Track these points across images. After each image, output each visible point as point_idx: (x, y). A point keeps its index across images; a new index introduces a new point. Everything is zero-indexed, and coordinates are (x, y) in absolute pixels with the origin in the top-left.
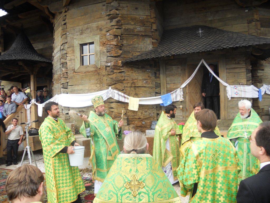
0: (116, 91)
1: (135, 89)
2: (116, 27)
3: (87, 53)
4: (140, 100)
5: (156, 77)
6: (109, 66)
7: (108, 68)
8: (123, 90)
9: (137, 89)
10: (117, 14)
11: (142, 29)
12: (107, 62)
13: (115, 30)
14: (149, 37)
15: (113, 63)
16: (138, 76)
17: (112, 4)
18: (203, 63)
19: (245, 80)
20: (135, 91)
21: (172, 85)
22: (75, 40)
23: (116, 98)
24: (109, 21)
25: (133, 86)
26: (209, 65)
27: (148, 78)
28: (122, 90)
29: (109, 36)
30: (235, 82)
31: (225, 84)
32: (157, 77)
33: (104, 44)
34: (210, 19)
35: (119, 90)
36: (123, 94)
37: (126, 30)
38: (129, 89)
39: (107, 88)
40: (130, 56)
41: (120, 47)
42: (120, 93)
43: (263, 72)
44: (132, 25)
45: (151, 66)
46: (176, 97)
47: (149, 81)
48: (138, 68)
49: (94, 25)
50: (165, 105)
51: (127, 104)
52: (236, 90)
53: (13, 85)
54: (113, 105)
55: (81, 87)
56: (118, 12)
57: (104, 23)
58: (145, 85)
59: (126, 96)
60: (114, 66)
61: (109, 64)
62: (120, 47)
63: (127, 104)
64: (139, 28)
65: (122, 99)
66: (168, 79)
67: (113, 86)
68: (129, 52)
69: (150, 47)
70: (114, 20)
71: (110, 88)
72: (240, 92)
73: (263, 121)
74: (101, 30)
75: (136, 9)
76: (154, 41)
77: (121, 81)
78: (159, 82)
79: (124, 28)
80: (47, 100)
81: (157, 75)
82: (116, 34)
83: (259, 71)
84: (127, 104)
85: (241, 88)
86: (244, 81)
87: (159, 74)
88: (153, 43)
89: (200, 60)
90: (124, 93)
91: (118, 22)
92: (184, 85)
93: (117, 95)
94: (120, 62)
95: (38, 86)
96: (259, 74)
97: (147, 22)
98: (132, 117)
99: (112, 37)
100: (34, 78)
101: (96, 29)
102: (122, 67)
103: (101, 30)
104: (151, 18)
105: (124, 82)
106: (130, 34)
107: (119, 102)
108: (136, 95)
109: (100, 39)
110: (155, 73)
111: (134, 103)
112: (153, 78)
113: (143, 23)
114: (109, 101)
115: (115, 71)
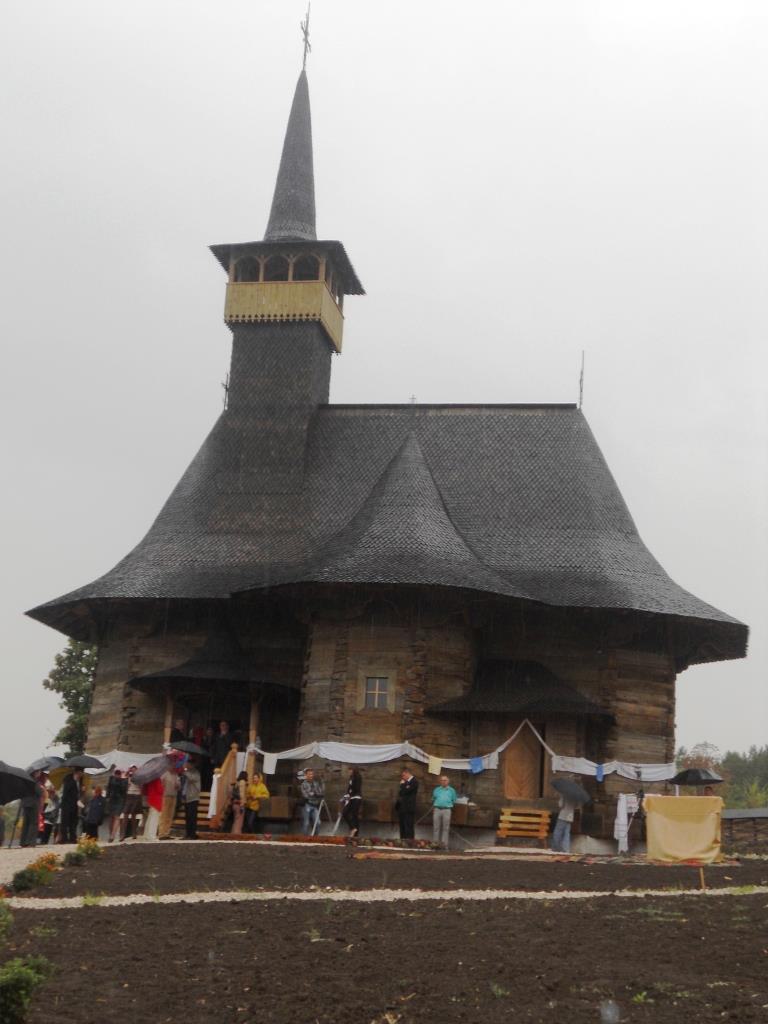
0: (414, 747)
2: (421, 663)
3: (374, 690)
5: (465, 734)
6: (407, 714)
7: (405, 716)
12: (405, 708)
15: (413, 711)
16: (442, 732)
18: (526, 724)
22: (360, 671)
23: (414, 755)
26: (533, 724)
30: (563, 753)
31: (551, 752)
33: (402, 683)
35: (417, 746)
36: (422, 752)
39: (403, 742)
41: (422, 690)
42: (419, 750)
46: (489, 764)
50: (475, 772)
52: (563, 763)
53: (727, 807)
54: (408, 765)
55: (362, 737)
59: (426, 754)
60: (414, 714)
61: (407, 711)
62: (422, 690)
66: (481, 739)
69: (460, 693)
70: (419, 653)
71: (407, 742)
72: (566, 766)
74: (399, 664)
76: (465, 684)
77: (421, 735)
80: (614, 814)
85: (569, 760)
86: (573, 751)
88: (465, 688)
90: (424, 751)
92: (500, 749)
93: (414, 752)
95: (733, 814)
96: (608, 746)
99: (415, 676)
103: (399, 664)
107: (416, 761)
108: (438, 755)
114: (405, 758)
115: (415, 721)
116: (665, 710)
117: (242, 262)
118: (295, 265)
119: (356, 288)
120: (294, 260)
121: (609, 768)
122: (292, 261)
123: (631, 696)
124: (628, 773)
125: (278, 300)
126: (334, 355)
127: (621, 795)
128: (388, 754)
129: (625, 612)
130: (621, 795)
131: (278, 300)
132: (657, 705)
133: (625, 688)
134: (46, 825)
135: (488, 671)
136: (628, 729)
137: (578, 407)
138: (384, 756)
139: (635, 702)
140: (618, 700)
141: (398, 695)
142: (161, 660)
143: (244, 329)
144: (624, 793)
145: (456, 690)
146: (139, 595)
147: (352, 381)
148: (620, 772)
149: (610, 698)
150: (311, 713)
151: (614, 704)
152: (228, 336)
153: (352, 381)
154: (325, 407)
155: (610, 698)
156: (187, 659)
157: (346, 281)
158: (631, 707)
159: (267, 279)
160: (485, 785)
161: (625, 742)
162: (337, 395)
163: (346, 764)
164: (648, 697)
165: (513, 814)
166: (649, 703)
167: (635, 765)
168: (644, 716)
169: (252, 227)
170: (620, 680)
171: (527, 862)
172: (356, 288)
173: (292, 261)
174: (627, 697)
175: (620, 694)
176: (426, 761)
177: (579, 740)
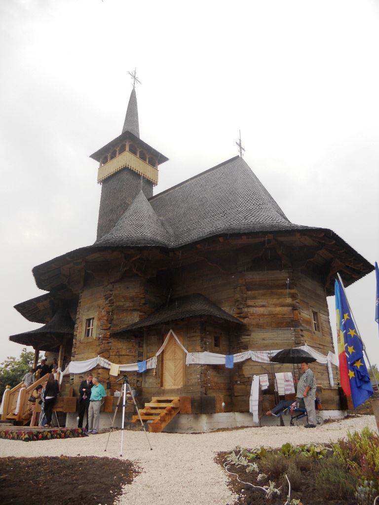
0: (103, 359)
1: (119, 357)
2: (109, 305)
4: (120, 367)
5: (140, 346)
8: (109, 358)
9: (121, 357)
10: (110, 295)
11: (131, 304)
13: (107, 307)
14: (137, 310)
17: (108, 287)
19: (200, 347)
20: (119, 359)
21: (151, 353)
24: (104, 300)
25: (118, 354)
27: (132, 348)
28: (108, 358)
29: (104, 313)
32: (140, 346)
34: (205, 286)
35: (105, 358)
37: (118, 307)
38: (113, 357)
40: (118, 328)
42: (105, 360)
43: (249, 337)
44: (123, 302)
45: (136, 337)
46: (151, 365)
47: (132, 350)
48: (123, 339)
49: (96, 304)
50: (141, 372)
51: (109, 370)
52: (193, 357)
54: (100, 371)
56: (111, 293)
57: (102, 301)
58: (128, 354)
59: (109, 362)
61: (101, 336)
63: (109, 370)
64: (128, 304)
65: (106, 366)
67: (101, 354)
68: (117, 325)
73: (371, 413)
75: (128, 288)
77: (108, 350)
78: (142, 351)
79: (115, 305)
80: (248, 394)
81: (141, 345)
82: (108, 311)
83: (243, 337)
84: (109, 369)
85: (196, 354)
86: (199, 348)
87: (143, 344)
89: (169, 330)
90: (109, 361)
91: (110, 301)
94: (109, 334)
96: (242, 340)
97: (136, 298)
98: (114, 383)
100: (62, 348)
101: (97, 306)
102: (109, 338)
104: (140, 294)
105: (111, 351)
106: (121, 310)
108: (120, 362)
109: (98, 315)
110: (139, 343)
111: (115, 369)
112: (137, 347)
113: (132, 299)
114: (98, 367)
115: (104, 342)
116: (291, 308)
119: (162, 159)
120: (118, 148)
121: (238, 358)
123: (259, 302)
124: (264, 360)
127: (255, 376)
128: (90, 366)
130: (255, 376)
133: (254, 298)
136: (259, 326)
137: (240, 156)
138: (89, 367)
139: (263, 306)
140: (249, 306)
141: (98, 327)
144: (257, 374)
145: (134, 318)
148: (254, 358)
149: (242, 306)
151: (246, 310)
155: (242, 306)
158: (261, 310)
160: (151, 380)
161: (257, 336)
163: (76, 374)
164: (275, 301)
165: (159, 401)
166: (276, 305)
167: (267, 352)
168: (273, 315)
170: (249, 293)
171: (54, 460)
172: (162, 159)
174: (256, 304)
175: (249, 303)
176: (109, 367)
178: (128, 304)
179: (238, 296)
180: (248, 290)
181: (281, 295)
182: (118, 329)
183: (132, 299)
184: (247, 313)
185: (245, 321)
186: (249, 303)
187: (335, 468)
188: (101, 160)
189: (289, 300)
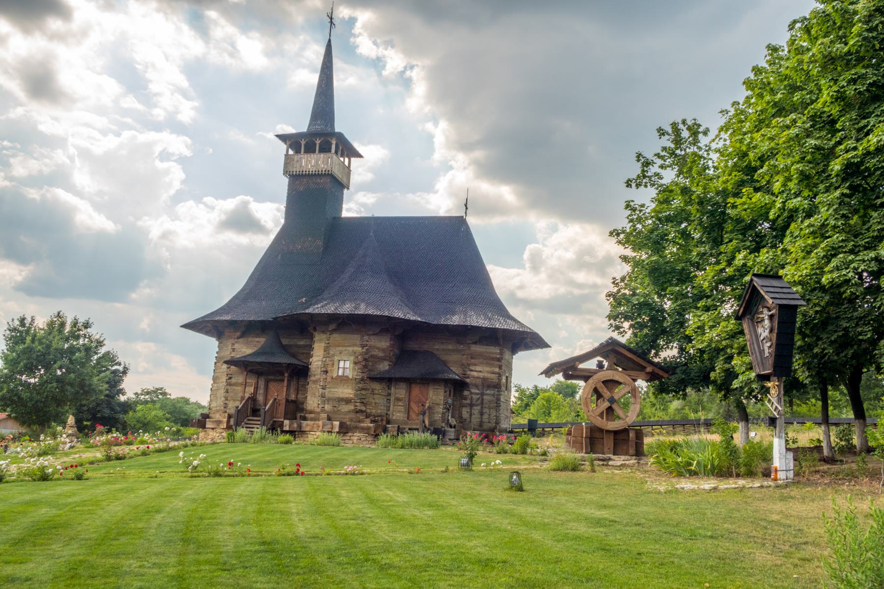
32: (389, 388)
117: (292, 141)
118: (305, 145)
122: (318, 142)
123: (478, 368)
125: (312, 163)
126: (345, 191)
129: (370, 333)
131: (312, 163)
132: (493, 373)
133: (475, 365)
134: (766, 455)
135: (403, 356)
140: (471, 370)
142: (245, 349)
143: (296, 178)
145: (384, 366)
146: (547, 297)
147: (354, 206)
150: (313, 378)
152: (286, 180)
153: (354, 206)
154: (340, 218)
156: (255, 349)
157: (350, 152)
159: (305, 152)
162: (345, 214)
164: (488, 369)
169: (300, 124)
173: (318, 142)
175: (472, 368)
177: (445, 392)
178: (381, 354)
179: (464, 362)
180: (472, 358)
181: (492, 365)
182: (373, 374)
183: (383, 350)
184: (637, 247)
185: (468, 380)
186: (472, 368)
187: (175, 217)
188: (288, 143)
189: (497, 370)
